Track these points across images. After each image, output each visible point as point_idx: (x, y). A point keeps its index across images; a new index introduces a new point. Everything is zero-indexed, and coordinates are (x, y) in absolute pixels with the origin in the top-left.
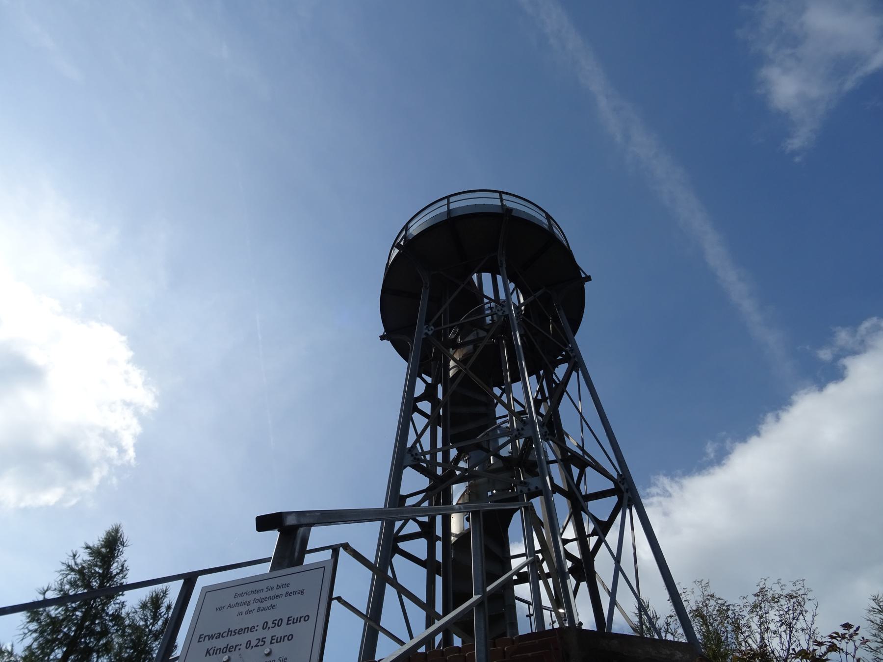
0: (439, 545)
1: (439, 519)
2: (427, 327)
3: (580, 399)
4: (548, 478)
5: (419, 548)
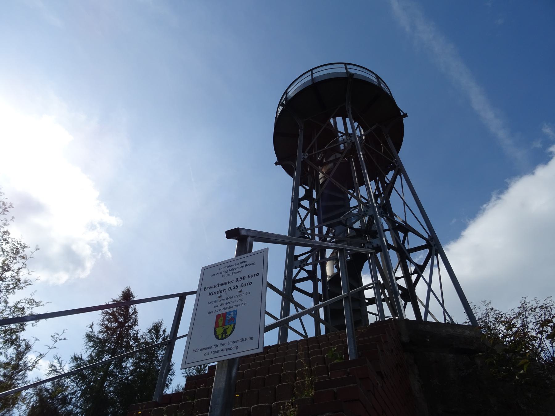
0: (320, 284)
1: (319, 267)
2: (304, 154)
3: (403, 192)
4: (384, 239)
5: (308, 286)
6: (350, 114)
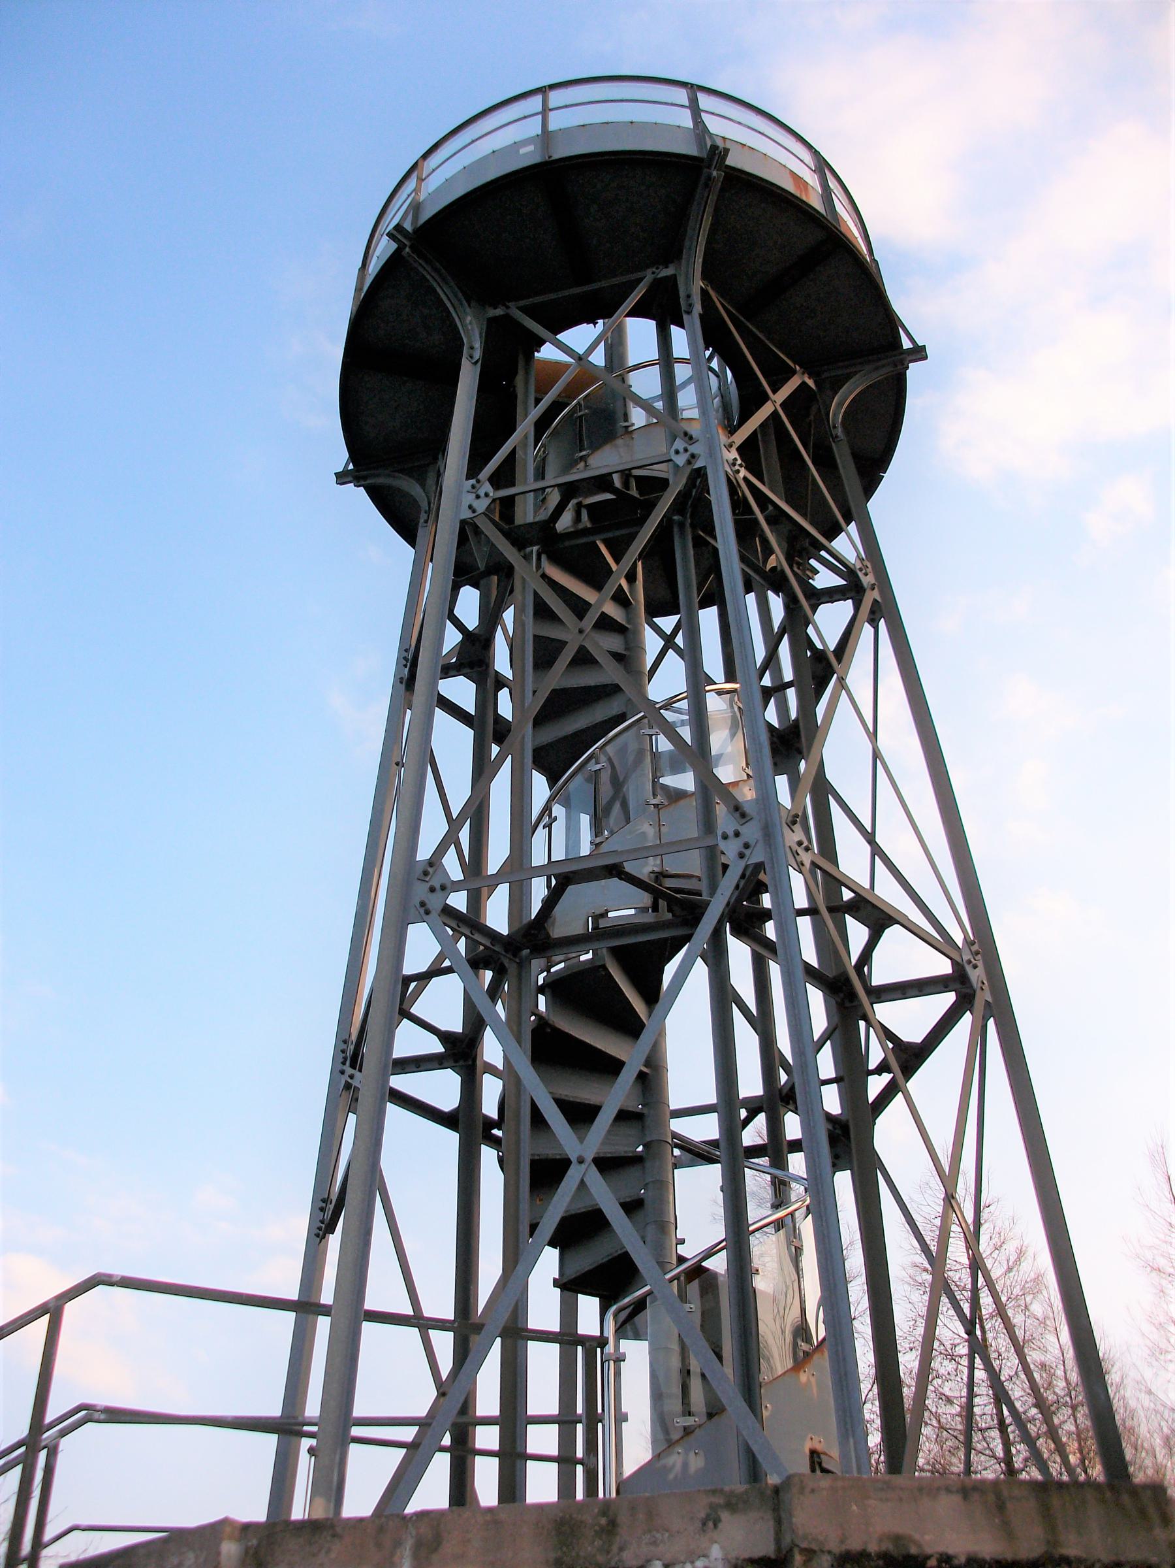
2: (473, 487)
6: (694, 319)
